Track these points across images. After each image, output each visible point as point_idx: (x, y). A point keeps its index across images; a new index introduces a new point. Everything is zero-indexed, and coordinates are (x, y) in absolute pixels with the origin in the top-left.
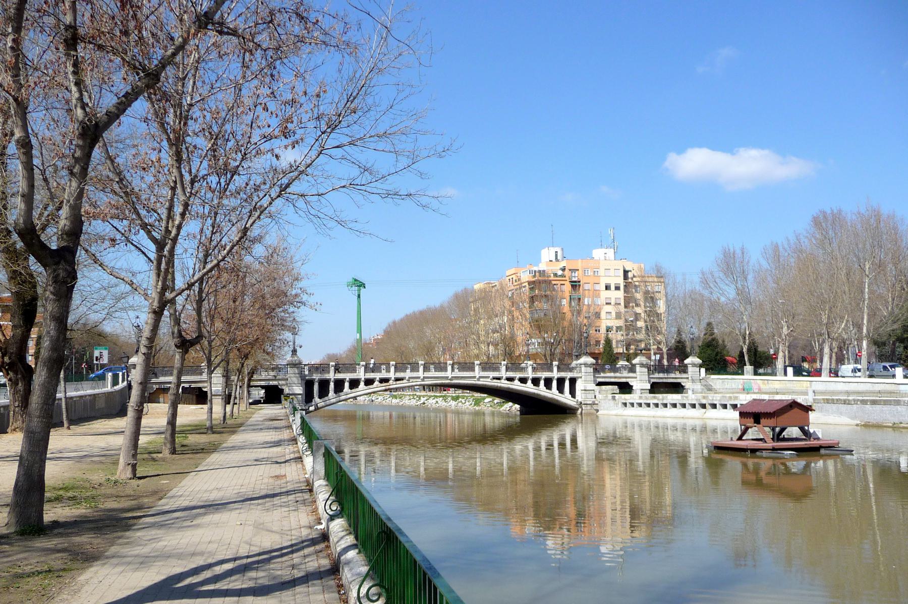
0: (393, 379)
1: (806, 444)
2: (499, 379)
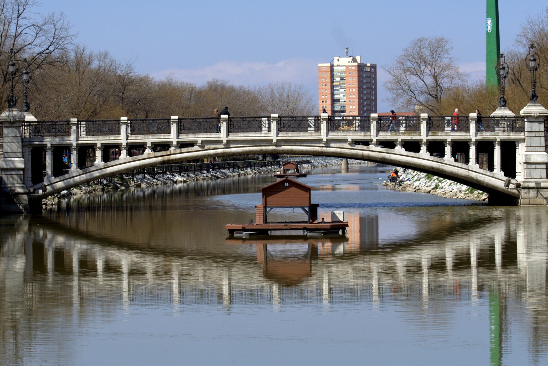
2: (366, 143)
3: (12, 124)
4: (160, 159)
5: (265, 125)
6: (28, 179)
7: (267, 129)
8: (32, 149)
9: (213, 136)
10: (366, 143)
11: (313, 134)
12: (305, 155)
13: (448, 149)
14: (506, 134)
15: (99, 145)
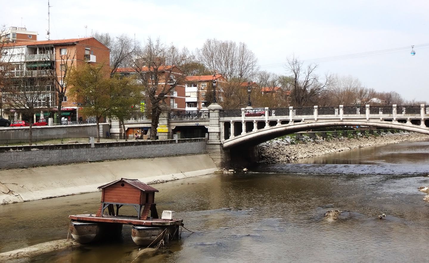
0: (291, 120)
1: (157, 223)
2: (391, 120)
3: (213, 111)
4: (284, 128)
5: (337, 110)
6: (223, 137)
7: (338, 113)
9: (310, 117)
10: (391, 120)
11: (382, 116)
12: (134, 123)
15: (255, 121)
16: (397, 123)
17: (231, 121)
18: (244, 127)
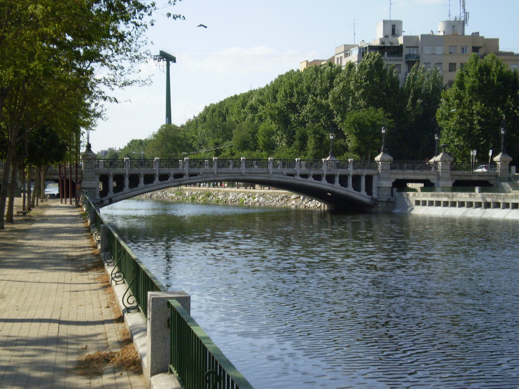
0: (187, 174)
2: (292, 175)
8: (431, 34)
10: (292, 175)
13: (337, 179)
14: (368, 171)
16: (299, 178)
17: (111, 174)
18: (127, 182)
